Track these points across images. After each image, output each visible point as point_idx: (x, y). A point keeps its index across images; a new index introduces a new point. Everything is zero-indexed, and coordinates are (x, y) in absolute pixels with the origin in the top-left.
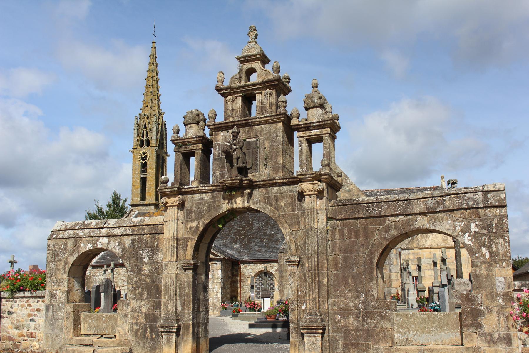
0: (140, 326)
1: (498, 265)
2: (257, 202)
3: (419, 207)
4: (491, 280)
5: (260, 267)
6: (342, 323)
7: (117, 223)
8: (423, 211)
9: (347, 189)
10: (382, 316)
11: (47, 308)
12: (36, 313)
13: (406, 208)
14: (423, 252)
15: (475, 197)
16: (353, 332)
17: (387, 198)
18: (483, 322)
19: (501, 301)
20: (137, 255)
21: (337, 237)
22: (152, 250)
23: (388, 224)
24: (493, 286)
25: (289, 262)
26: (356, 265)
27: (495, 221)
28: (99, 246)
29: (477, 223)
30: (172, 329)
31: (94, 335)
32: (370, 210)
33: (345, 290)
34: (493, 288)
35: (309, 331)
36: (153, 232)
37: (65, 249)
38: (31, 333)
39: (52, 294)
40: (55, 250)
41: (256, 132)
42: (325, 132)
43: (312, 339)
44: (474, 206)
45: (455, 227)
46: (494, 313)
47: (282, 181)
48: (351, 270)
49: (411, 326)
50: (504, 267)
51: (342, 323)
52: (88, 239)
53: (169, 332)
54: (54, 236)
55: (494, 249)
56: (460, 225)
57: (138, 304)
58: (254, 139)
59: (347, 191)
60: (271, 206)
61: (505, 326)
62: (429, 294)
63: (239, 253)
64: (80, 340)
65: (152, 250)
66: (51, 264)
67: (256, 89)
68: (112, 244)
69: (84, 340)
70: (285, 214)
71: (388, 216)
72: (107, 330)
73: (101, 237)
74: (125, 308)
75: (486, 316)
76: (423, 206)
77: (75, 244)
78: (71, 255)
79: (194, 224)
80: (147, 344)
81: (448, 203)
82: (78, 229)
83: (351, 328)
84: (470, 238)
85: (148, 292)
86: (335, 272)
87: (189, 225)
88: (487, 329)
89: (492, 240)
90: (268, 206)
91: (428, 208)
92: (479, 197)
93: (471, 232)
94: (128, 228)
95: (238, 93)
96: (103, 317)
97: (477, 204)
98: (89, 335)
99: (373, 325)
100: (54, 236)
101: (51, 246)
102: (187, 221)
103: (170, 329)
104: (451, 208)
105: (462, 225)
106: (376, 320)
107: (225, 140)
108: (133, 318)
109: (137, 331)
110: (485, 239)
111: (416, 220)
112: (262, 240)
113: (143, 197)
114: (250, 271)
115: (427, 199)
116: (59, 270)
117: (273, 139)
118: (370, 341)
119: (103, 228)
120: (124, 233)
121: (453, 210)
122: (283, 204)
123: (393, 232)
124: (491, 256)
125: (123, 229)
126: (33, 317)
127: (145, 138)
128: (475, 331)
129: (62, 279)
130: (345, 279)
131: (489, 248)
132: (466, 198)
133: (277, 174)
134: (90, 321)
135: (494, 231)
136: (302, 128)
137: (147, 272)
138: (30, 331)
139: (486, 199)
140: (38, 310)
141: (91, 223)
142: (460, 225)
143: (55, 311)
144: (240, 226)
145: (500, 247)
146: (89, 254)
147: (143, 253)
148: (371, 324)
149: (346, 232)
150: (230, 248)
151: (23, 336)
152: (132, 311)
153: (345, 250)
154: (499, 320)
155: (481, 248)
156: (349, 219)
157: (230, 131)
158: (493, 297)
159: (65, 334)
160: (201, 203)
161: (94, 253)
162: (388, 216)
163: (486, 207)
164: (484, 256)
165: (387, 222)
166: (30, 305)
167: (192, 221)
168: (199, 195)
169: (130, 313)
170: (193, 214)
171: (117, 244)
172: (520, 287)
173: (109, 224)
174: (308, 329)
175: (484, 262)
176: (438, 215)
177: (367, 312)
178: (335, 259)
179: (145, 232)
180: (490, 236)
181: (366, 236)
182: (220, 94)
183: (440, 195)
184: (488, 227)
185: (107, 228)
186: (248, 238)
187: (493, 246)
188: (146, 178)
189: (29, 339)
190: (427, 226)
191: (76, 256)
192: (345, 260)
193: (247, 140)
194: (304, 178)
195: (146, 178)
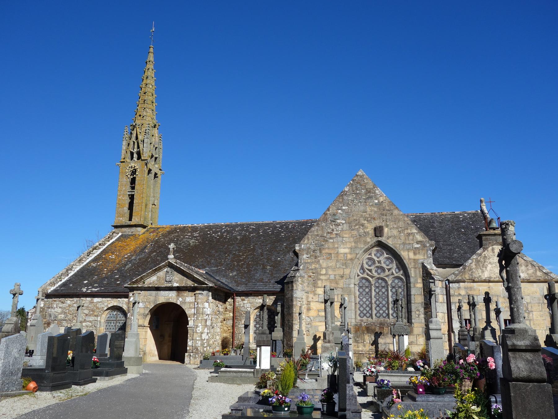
9: (377, 201)
14: (480, 286)
59: (376, 204)
63: (235, 282)
112: (264, 268)
113: (130, 219)
127: (136, 150)
144: (239, 251)
150: (224, 276)
186: (248, 264)
188: (134, 195)
195: (134, 195)
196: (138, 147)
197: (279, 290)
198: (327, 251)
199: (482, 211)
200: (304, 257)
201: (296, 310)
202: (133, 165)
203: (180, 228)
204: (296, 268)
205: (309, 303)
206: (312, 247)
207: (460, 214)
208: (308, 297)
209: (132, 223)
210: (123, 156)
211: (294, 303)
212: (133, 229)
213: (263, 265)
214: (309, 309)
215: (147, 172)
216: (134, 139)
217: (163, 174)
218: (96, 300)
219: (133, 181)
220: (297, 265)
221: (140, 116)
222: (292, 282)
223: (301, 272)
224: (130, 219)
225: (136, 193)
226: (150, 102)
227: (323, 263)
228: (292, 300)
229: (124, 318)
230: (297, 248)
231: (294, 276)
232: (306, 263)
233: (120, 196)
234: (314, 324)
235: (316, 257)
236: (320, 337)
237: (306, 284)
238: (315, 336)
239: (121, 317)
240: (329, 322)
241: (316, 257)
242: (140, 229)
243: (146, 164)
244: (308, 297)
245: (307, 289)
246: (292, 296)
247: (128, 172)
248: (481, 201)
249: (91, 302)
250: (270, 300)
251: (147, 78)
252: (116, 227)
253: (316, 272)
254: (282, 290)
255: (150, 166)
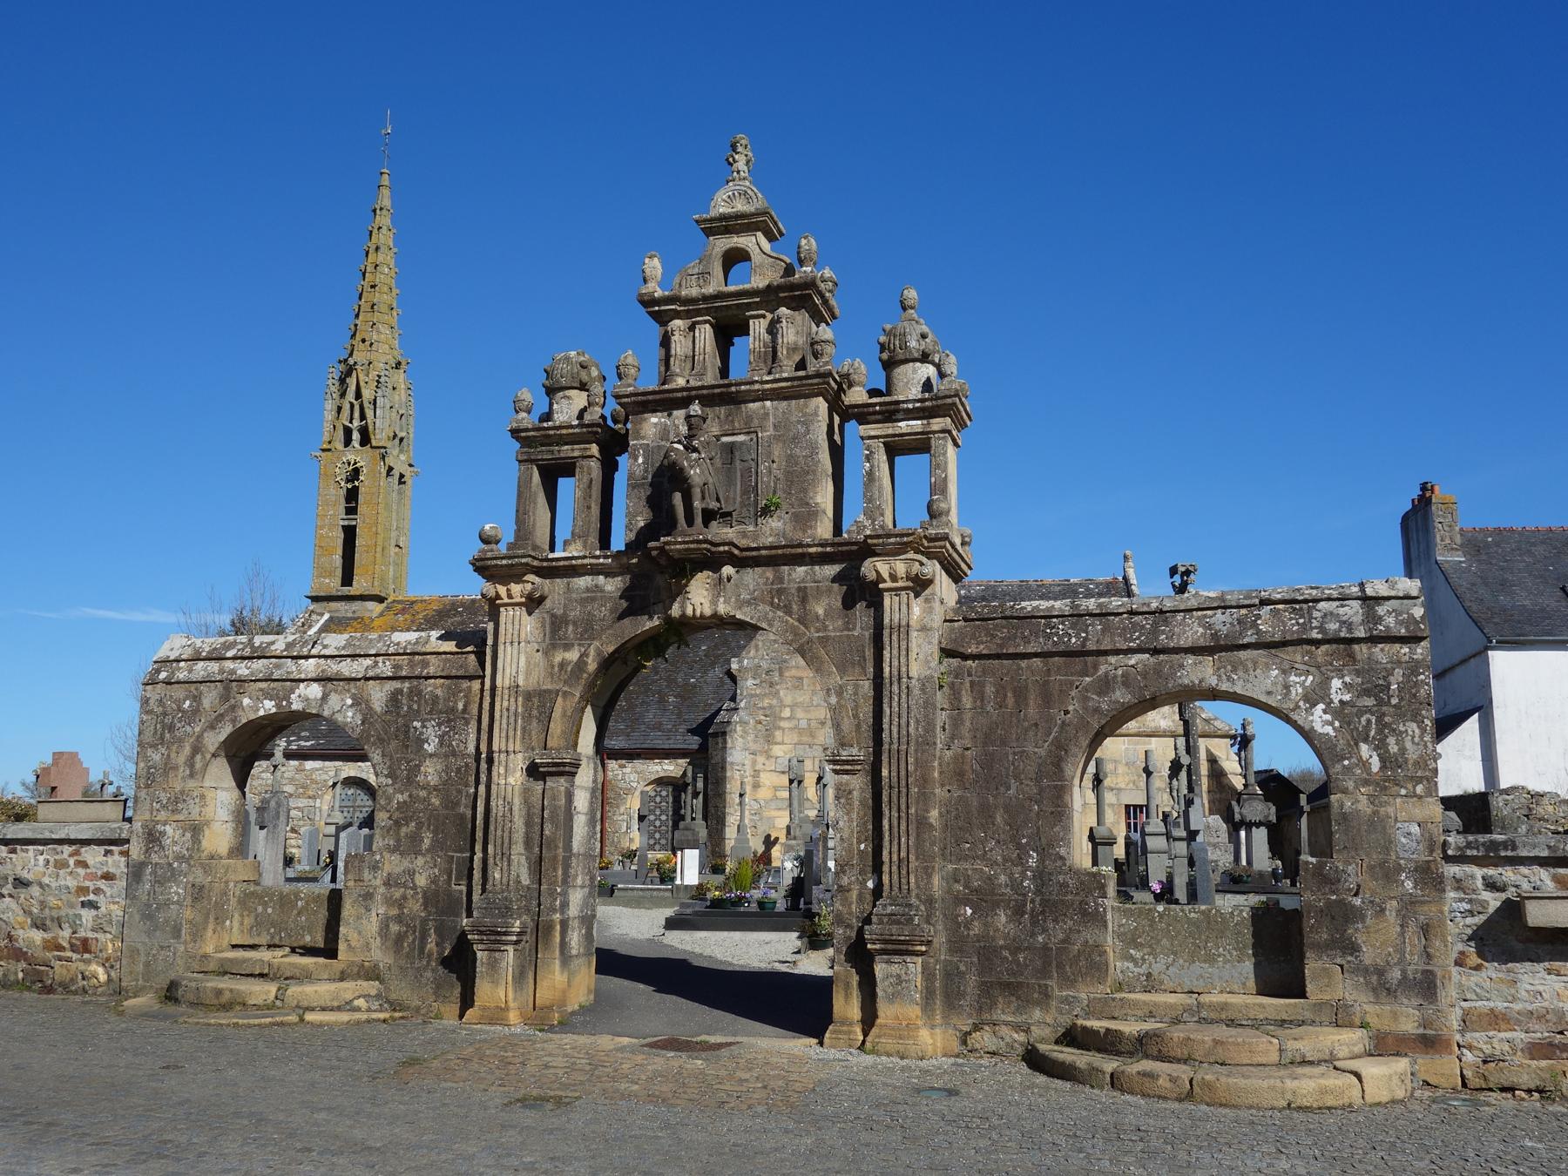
0: (408, 926)
1: (1403, 792)
2: (748, 603)
3: (1192, 632)
4: (1384, 828)
5: (658, 768)
6: (976, 928)
7: (348, 644)
8: (1202, 643)
10: (1084, 913)
11: (136, 873)
12: (102, 884)
13: (1155, 631)
15: (1341, 611)
16: (1006, 953)
17: (1100, 605)
18: (1360, 939)
19: (1409, 885)
20: (407, 732)
21: (967, 701)
22: (449, 721)
23: (1106, 674)
24: (1388, 845)
25: (834, 762)
26: (1016, 777)
27: (1398, 674)
28: (296, 706)
29: (1347, 679)
30: (505, 934)
31: (269, 946)
32: (1057, 634)
33: (983, 842)
34: (1387, 850)
35: (890, 947)
36: (454, 672)
37: (196, 711)
38: (85, 941)
39: (150, 834)
40: (165, 714)
41: (749, 419)
42: (935, 428)
43: (895, 969)
44: (1342, 635)
45: (1287, 687)
46: (1391, 915)
47: (820, 549)
48: (1002, 789)
49: (1159, 941)
50: (1420, 797)
51: (976, 928)
52: (263, 685)
53: (499, 942)
54: (163, 675)
55: (1393, 748)
56: (1302, 684)
57: (406, 864)
58: (741, 438)
60: (788, 612)
61: (1420, 948)
62: (1127, 853)
64: (231, 960)
65: (449, 721)
66: (149, 752)
67: (749, 306)
68: (334, 701)
69: (245, 961)
70: (827, 638)
71: (1106, 653)
72: (310, 933)
73: (303, 681)
74: (366, 875)
75: (1368, 921)
76: (1201, 630)
77: (225, 697)
78: (212, 727)
79: (573, 655)
80: (429, 974)
81: (1266, 624)
82: (234, 658)
83: (1001, 942)
84: (1328, 717)
85: (435, 832)
86: (959, 793)
87: (558, 657)
88: (1368, 956)
89: (1386, 725)
90: (780, 613)
91: (1215, 636)
92: (1353, 610)
93: (1332, 701)
94: (380, 659)
95: (699, 313)
96: (297, 898)
97: (1350, 630)
98: (253, 947)
99: (1061, 936)
100: (163, 675)
101: (152, 702)
102: (554, 646)
103: (499, 933)
104: (1277, 638)
105: (1308, 683)
106: (1070, 923)
107: (664, 433)
108: (389, 901)
109: (400, 939)
110: (1369, 721)
111: (1182, 666)
112: (662, 700)
113: (347, 580)
114: (634, 777)
115: (1209, 613)
116: (176, 768)
117: (795, 439)
118: (1050, 977)
119: (306, 657)
120: (370, 674)
121: (1284, 644)
122: (821, 611)
123: (1118, 693)
124: (1383, 767)
125: (368, 662)
126: (92, 897)
127: (356, 423)
128: (1339, 961)
129: (182, 792)
130: (986, 811)
131: (1380, 747)
132: (1316, 614)
133: (804, 531)
134: (260, 909)
135: (1394, 701)
136: (875, 413)
137: (433, 779)
138: (82, 934)
139: (1372, 618)
140: (108, 877)
141: (273, 643)
142: (1302, 684)
143: (160, 882)
145: (1408, 745)
146: (263, 727)
147: (424, 726)
148: (1057, 932)
149: (989, 690)
151: (60, 948)
152: (387, 884)
153: (986, 736)
154: (1402, 934)
155: (1357, 744)
156: (998, 656)
157: (679, 414)
158: (1388, 873)
159: (185, 943)
160: (593, 599)
161: (282, 723)
162: (1106, 653)
163: (1373, 640)
164: (1366, 765)
165: (1103, 669)
166: (84, 865)
167: (568, 647)
168: (589, 578)
169: (382, 890)
170: (571, 628)
171: (349, 702)
172: (1460, 849)
173: (325, 647)
174: (886, 942)
175: (1366, 783)
176: (1243, 654)
177: (1044, 903)
178: (959, 760)
179: (432, 670)
180: (1384, 714)
181: (1047, 699)
182: (650, 313)
183: (1247, 602)
184: (1377, 690)
185: (320, 657)
187: (1391, 740)
189: (75, 956)
190: (1213, 681)
191: (226, 730)
192: (988, 762)
193: (725, 439)
194: (883, 544)
196: (363, 417)
197: (695, 747)
198: (794, 672)
199: (1125, 578)
200: (748, 684)
201: (732, 788)
202: (352, 458)
203: (462, 604)
204: (733, 705)
205: (756, 773)
206: (764, 665)
207: (1081, 585)
208: (754, 762)
209: (354, 590)
210: (326, 437)
211: (728, 774)
212: (356, 605)
213: (659, 692)
214: (756, 786)
215: (384, 471)
216: (351, 395)
217: (417, 474)
218: (309, 765)
219: (352, 496)
220: (733, 699)
221: (364, 341)
222: (724, 733)
223: (741, 713)
224: (347, 580)
225: (361, 522)
226: (384, 309)
227: (787, 697)
228: (724, 769)
229: (370, 803)
230: (734, 666)
231: (729, 722)
232: (752, 696)
233: (322, 528)
234: (766, 814)
235: (771, 685)
236: (777, 839)
237: (751, 738)
238: (769, 836)
239: (363, 799)
240: (796, 811)
241: (771, 685)
242: (371, 605)
243: (383, 458)
244: (754, 762)
245: (753, 746)
246: (724, 760)
247: (341, 473)
248: (1126, 558)
249: (299, 770)
250: (671, 768)
251: (377, 249)
252: (315, 599)
253: (772, 715)
254: (704, 748)
255: (390, 461)
